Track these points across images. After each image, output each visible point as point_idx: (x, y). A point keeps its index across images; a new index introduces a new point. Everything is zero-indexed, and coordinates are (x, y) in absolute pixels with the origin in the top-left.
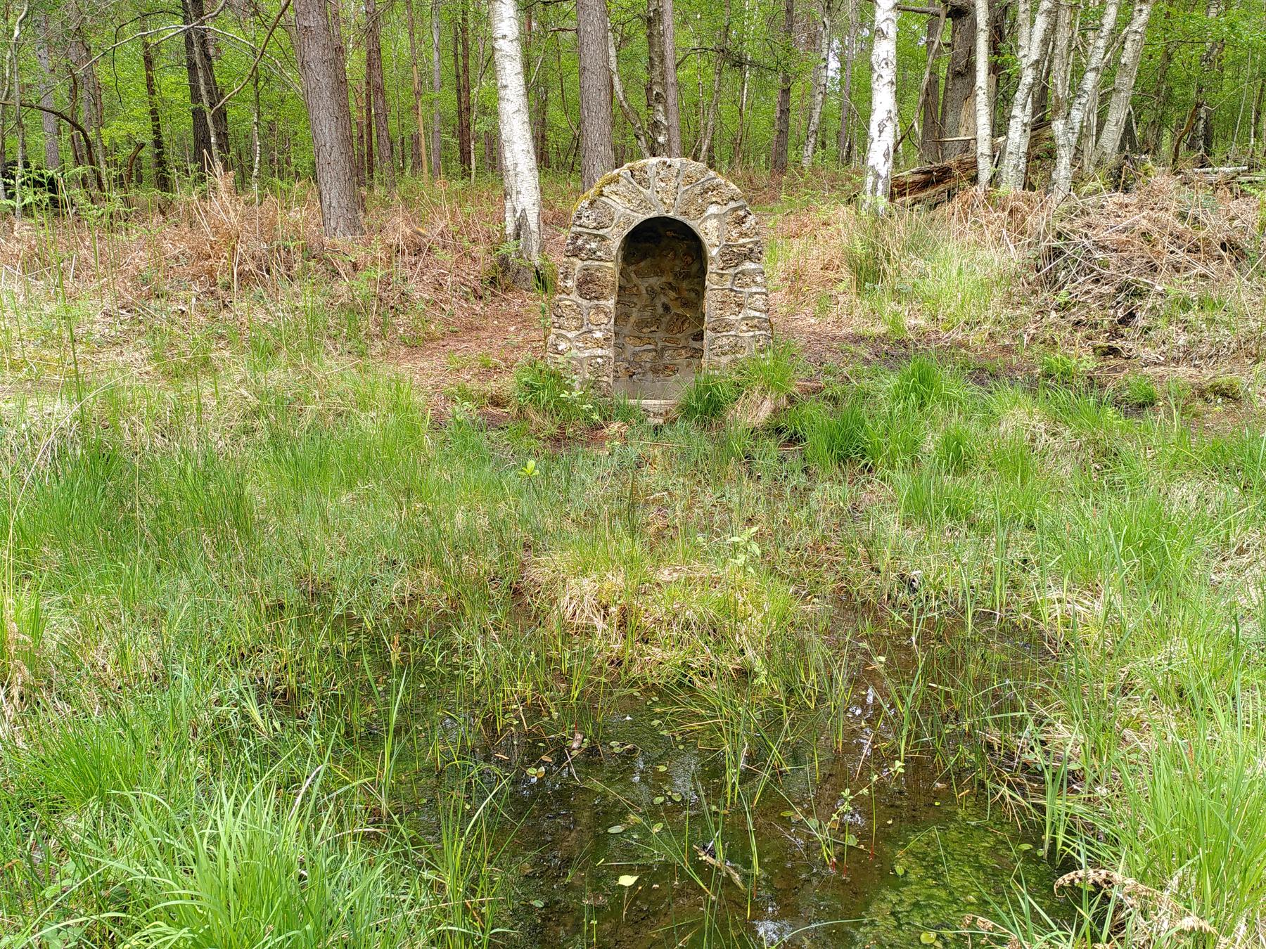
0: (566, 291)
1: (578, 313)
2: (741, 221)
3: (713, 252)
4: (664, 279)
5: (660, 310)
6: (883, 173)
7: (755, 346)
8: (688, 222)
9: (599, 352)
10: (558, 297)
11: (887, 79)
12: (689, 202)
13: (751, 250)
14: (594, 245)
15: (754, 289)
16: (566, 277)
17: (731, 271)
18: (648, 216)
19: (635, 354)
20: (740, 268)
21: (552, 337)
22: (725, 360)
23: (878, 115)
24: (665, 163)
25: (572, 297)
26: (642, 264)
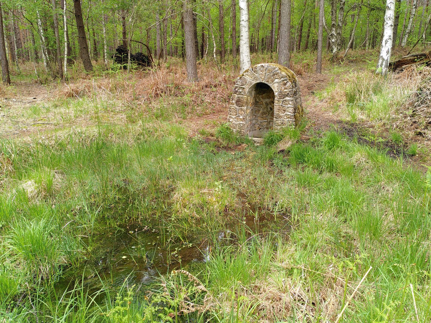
0: (232, 104)
1: (236, 111)
2: (285, 84)
3: (276, 94)
4: (270, 100)
5: (269, 109)
6: (386, 58)
7: (289, 124)
8: (269, 84)
9: (241, 122)
10: (230, 105)
11: (389, 24)
12: (269, 78)
13: (288, 94)
14: (241, 90)
15: (289, 106)
16: (233, 100)
17: (282, 100)
18: (257, 82)
19: (261, 123)
20: (285, 99)
21: (228, 117)
22: (279, 127)
23: (386, 37)
24: (262, 66)
25: (234, 106)
26: (264, 95)
